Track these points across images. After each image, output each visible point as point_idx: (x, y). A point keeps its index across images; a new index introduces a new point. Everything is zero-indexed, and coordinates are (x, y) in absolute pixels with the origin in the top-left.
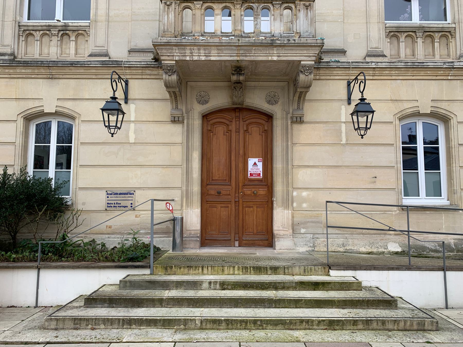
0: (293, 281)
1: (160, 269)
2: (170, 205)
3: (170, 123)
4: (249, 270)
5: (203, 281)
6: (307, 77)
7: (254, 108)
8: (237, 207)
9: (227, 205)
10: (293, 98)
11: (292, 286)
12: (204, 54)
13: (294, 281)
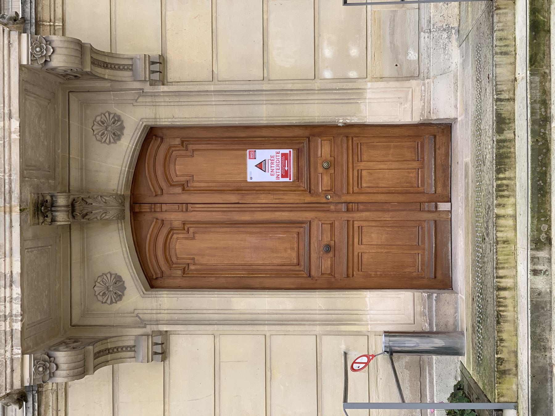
0: (528, 81)
1: (505, 386)
2: (356, 361)
3: (167, 362)
4: (505, 182)
5: (531, 288)
6: (58, 50)
7: (132, 171)
8: (361, 207)
9: (356, 229)
10: (107, 79)
11: (541, 82)
12: (8, 289)
13: (528, 78)
